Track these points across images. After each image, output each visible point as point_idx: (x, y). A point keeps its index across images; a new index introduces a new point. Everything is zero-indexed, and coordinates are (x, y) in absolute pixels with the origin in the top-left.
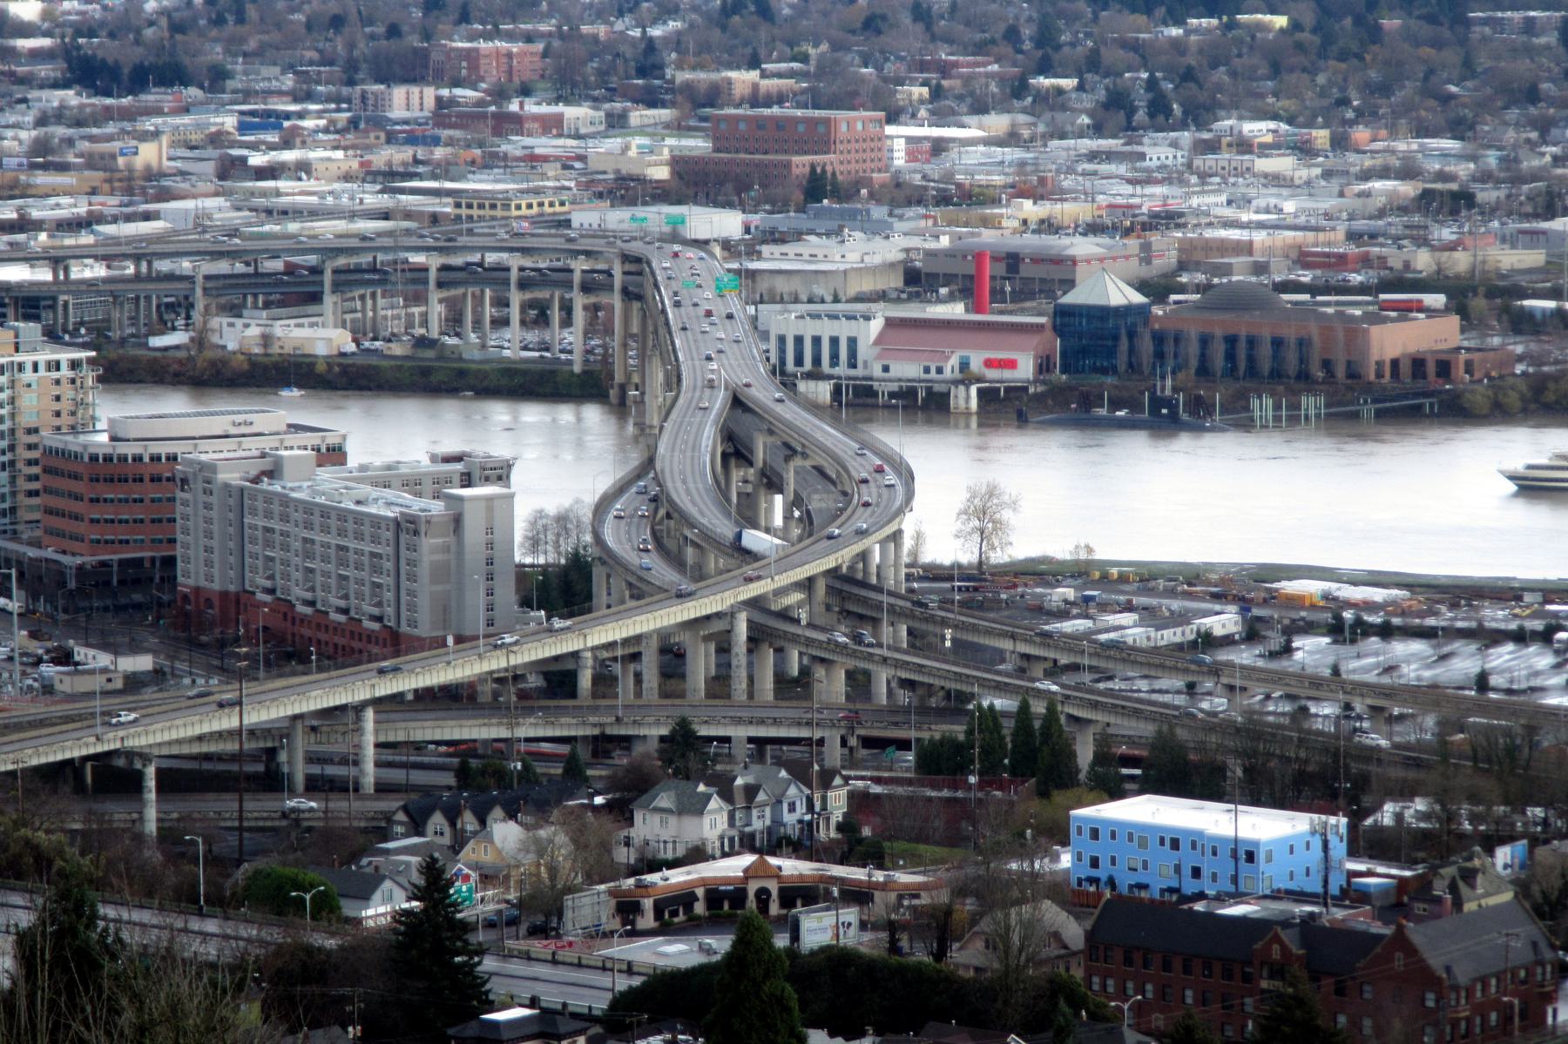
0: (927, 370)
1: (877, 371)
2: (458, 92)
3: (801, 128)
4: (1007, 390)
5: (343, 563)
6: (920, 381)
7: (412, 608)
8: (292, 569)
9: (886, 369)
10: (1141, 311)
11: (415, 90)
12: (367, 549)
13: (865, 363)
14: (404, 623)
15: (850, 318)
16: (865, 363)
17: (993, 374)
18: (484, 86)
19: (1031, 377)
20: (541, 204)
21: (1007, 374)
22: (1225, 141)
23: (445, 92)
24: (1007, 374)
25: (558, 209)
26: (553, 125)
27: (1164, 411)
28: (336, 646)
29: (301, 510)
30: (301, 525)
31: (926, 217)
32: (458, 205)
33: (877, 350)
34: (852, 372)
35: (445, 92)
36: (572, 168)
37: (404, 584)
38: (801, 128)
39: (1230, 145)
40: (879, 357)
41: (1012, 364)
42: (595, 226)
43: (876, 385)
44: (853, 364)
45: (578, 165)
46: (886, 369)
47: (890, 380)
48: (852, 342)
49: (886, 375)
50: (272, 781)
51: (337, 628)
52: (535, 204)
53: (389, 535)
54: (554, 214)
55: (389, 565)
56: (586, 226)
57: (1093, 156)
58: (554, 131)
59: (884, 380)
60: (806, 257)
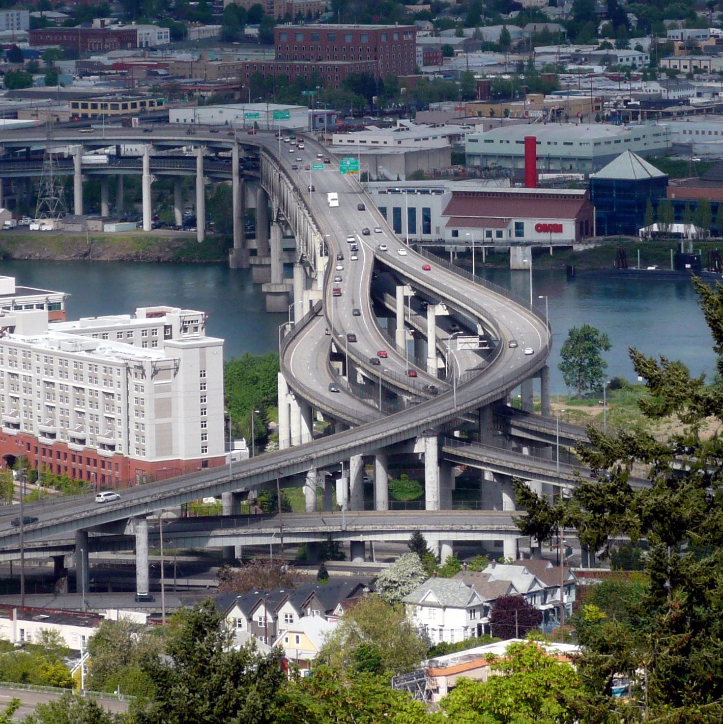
0: (489, 234)
1: (448, 235)
2: (48, 14)
3: (348, 39)
4: (555, 249)
5: (79, 401)
6: (484, 243)
7: (140, 437)
8: (34, 408)
9: (455, 234)
10: (659, 184)
11: (15, 12)
12: (71, 384)
13: (438, 228)
14: (133, 450)
15: (425, 192)
16: (438, 228)
17: (544, 237)
18: (68, 8)
19: (574, 238)
20: (143, 104)
21: (556, 237)
22: (678, 44)
23: (37, 14)
24: (556, 237)
25: (157, 108)
26: (127, 40)
27: (688, 266)
28: (74, 470)
29: (42, 358)
30: (43, 371)
31: (461, 109)
32: (75, 106)
33: (447, 219)
34: (427, 237)
35: (37, 14)
36: (157, 74)
37: (134, 418)
38: (348, 39)
39: (681, 48)
40: (448, 225)
41: (558, 229)
42: (189, 121)
43: (447, 247)
44: (427, 230)
45: (161, 72)
46: (455, 234)
47: (460, 243)
48: (427, 212)
49: (455, 238)
50: (338, 649)
51: (75, 456)
52: (138, 103)
53: (121, 378)
54: (154, 111)
55: (121, 403)
56: (181, 121)
57: (575, 58)
58: (129, 45)
59: (454, 243)
60: (369, 143)
